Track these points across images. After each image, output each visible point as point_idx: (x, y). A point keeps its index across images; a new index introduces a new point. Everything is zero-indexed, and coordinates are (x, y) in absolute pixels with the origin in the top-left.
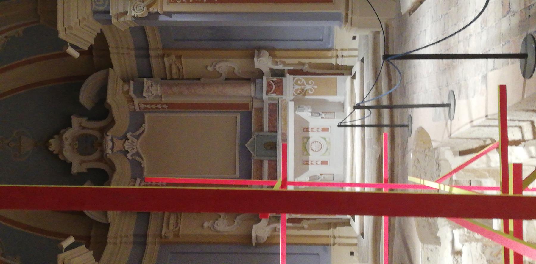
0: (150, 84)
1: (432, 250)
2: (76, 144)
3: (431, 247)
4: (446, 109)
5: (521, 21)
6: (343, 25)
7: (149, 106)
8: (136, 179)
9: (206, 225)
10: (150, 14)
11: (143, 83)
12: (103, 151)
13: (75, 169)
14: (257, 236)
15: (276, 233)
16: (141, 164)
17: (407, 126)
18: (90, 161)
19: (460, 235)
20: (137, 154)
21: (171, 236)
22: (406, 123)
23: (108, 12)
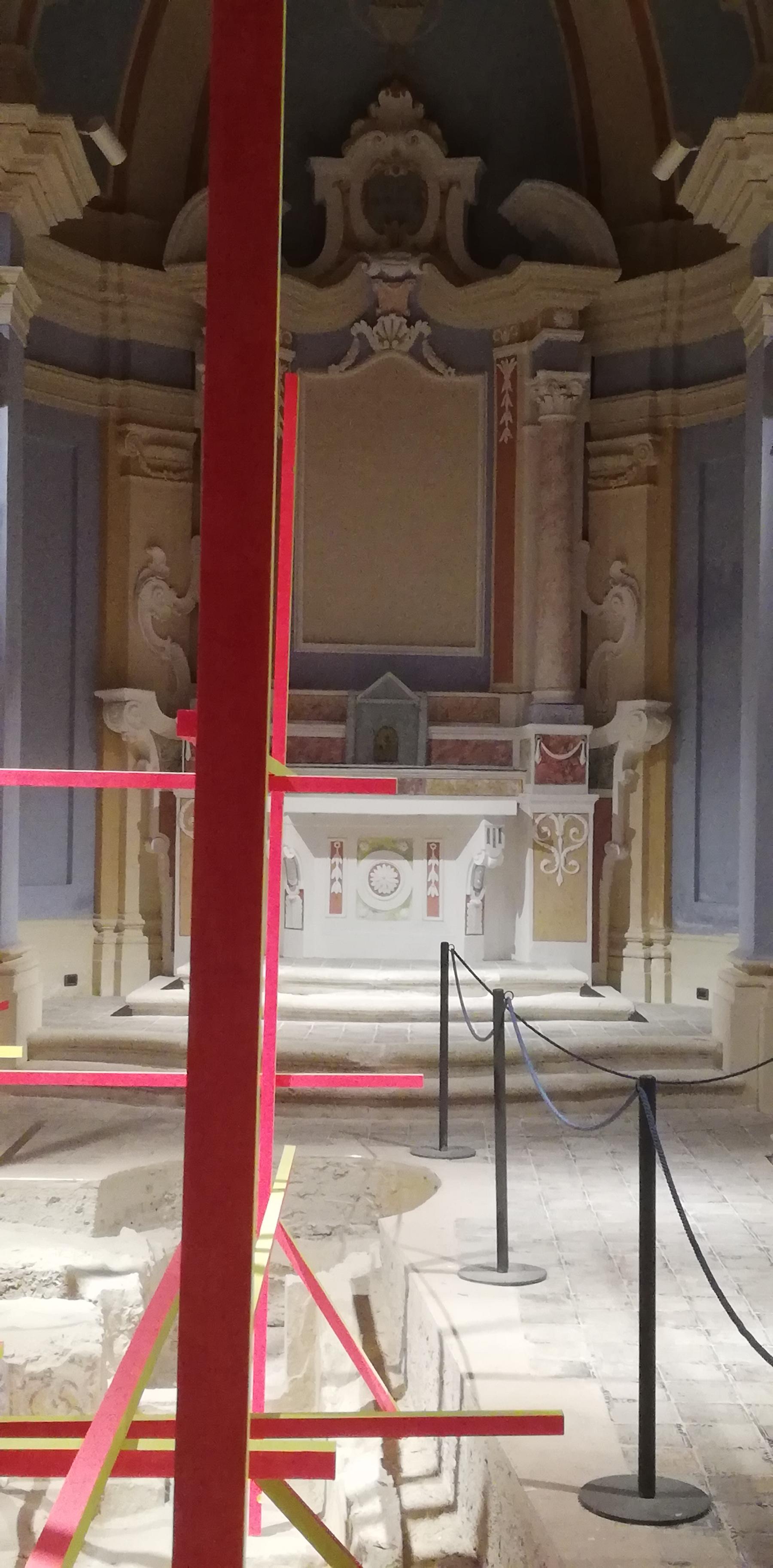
1: (80, 1211)
2: (396, 170)
3: (91, 1209)
6: (740, 962)
7: (507, 386)
9: (157, 553)
12: (376, 250)
15: (131, 760)
17: (443, 1144)
20: (366, 352)
21: (126, 450)
22: (451, 1141)
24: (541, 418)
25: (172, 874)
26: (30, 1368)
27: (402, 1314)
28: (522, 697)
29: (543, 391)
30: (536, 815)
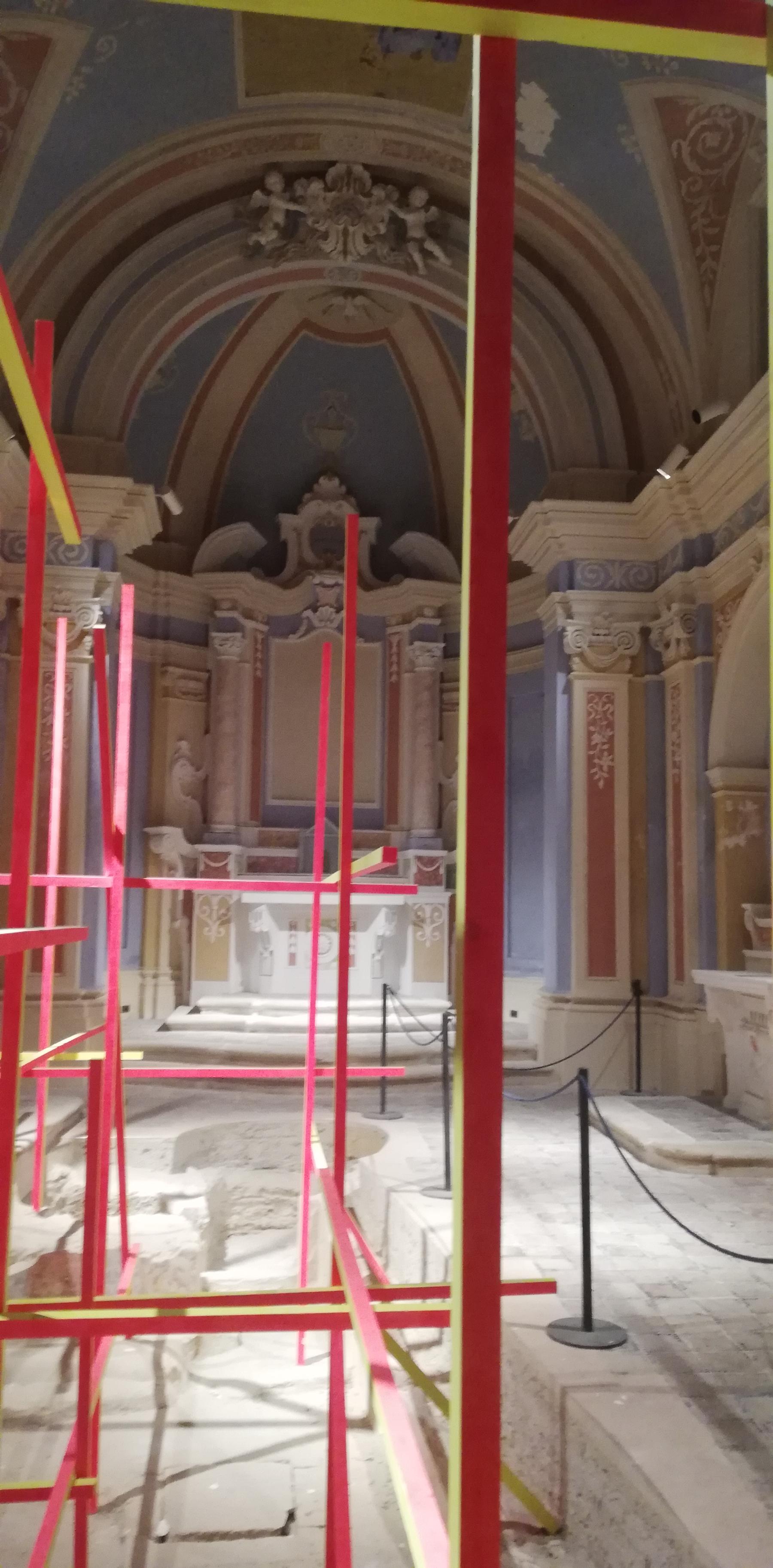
0: (434, 654)
1: (162, 1157)
2: (329, 523)
3: (170, 1155)
4: (442, 1182)
5: (644, 1319)
6: (548, 995)
7: (395, 649)
8: (267, 623)
9: (184, 744)
10: (569, 657)
11: (434, 640)
12: (318, 568)
13: (287, 520)
14: (164, 835)
15: (165, 870)
16: (294, 632)
17: (383, 1110)
18: (300, 544)
19: (196, 1210)
20: (311, 628)
21: (167, 682)
22: (389, 1107)
23: (571, 587)
24: (417, 669)
25: (190, 940)
26: (156, 1260)
27: (383, 1218)
28: (404, 833)
29: (418, 653)
30: (415, 904)
